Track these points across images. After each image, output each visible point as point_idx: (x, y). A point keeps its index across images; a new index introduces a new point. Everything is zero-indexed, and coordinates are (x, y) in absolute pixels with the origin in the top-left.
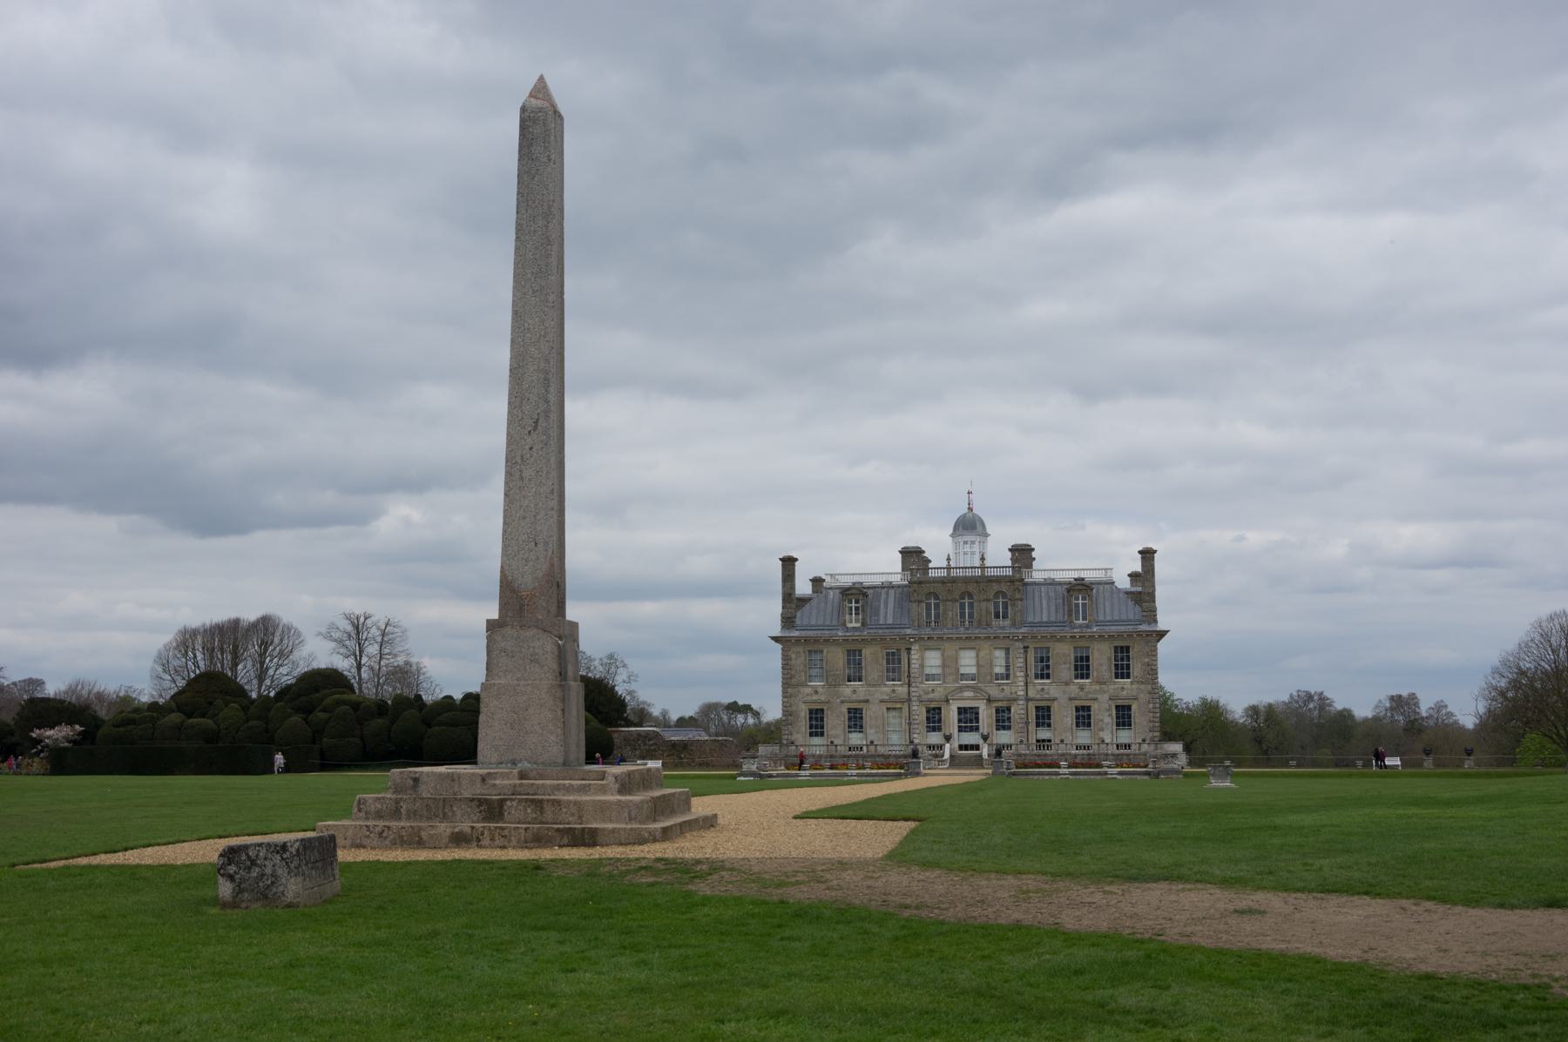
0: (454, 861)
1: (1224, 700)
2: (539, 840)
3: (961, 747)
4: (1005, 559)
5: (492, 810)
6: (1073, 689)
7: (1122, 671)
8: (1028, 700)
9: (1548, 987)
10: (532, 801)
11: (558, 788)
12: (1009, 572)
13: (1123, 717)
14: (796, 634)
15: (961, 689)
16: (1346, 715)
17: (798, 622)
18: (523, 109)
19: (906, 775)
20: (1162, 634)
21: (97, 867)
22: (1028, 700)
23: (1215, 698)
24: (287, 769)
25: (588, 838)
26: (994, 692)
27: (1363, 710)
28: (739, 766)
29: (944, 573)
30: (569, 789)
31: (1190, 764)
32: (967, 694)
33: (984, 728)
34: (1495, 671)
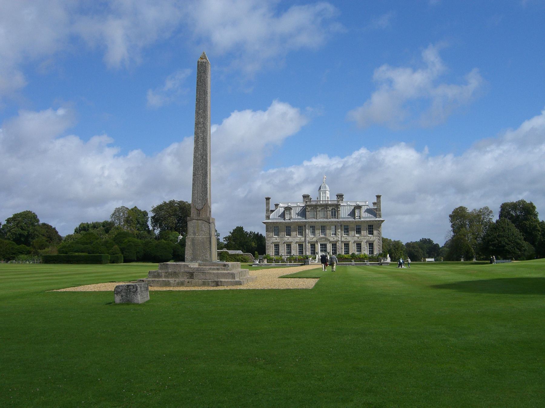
0: (230, 290)
1: (401, 241)
2: (204, 284)
4: (335, 198)
5: (191, 275)
6: (356, 239)
7: (371, 233)
8: (342, 242)
9: (504, 246)
11: (210, 269)
12: (336, 202)
14: (271, 221)
16: (437, 245)
17: (271, 217)
19: (304, 265)
20: (383, 221)
21: (78, 292)
22: (342, 242)
25: (217, 284)
26: (332, 239)
30: (214, 269)
31: (391, 261)
32: (323, 240)
34: (475, 210)
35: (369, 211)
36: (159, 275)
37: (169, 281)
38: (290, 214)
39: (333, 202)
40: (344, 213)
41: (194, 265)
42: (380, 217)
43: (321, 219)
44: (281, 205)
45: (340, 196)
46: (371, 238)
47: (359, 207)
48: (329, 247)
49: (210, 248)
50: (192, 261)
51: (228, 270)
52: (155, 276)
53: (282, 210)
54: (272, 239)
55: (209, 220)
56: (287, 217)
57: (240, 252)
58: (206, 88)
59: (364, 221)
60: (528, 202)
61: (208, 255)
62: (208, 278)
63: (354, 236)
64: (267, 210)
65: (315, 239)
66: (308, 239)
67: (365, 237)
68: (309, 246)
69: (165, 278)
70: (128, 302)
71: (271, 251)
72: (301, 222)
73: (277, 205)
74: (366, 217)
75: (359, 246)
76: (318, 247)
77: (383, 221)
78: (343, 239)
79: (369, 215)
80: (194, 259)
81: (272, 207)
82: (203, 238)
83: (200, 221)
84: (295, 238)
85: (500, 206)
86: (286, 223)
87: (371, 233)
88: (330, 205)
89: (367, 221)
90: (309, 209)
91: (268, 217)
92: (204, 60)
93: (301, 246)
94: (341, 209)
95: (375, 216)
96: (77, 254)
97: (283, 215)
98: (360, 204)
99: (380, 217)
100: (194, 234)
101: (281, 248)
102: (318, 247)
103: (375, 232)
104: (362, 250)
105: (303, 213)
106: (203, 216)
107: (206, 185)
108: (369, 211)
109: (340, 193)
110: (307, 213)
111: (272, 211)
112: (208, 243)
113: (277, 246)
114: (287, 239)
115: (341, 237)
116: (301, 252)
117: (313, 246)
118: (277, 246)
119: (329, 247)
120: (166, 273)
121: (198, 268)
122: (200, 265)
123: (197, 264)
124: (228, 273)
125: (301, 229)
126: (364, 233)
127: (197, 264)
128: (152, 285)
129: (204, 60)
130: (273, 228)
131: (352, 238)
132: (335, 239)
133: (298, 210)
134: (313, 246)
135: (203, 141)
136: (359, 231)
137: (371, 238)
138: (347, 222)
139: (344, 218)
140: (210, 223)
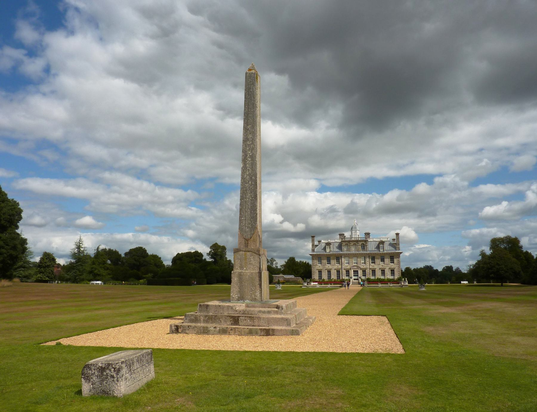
3: (354, 279)
4: (363, 236)
6: (381, 266)
8: (370, 269)
10: (250, 317)
11: (260, 311)
12: (364, 239)
13: (393, 272)
15: (354, 266)
16: (437, 270)
18: (246, 73)
20: (401, 253)
22: (370, 269)
23: (6, 192)
24: (197, 284)
26: (362, 267)
27: (440, 269)
28: (303, 284)
29: (349, 239)
30: (264, 312)
33: (360, 275)
35: (391, 245)
36: (196, 320)
37: (207, 327)
38: (330, 248)
39: (362, 239)
40: (371, 248)
41: (240, 306)
42: (399, 250)
43: (353, 250)
44: (323, 241)
45: (367, 234)
46: (392, 265)
47: (382, 242)
48: (360, 273)
49: (260, 285)
50: (238, 300)
51: (281, 313)
52: (192, 321)
53: (323, 245)
54: (317, 266)
55: (259, 251)
56: (328, 250)
57: (292, 277)
58: (255, 101)
59: (387, 253)
60: (513, 237)
61: (258, 294)
62: (256, 323)
63: (379, 265)
64: (313, 245)
65: (349, 267)
66: (343, 267)
67: (388, 265)
68: (344, 272)
69: (204, 323)
70: (105, 394)
71: (316, 276)
72: (338, 254)
73: (319, 242)
74: (387, 249)
75: (383, 272)
76: (352, 273)
77: (401, 253)
78: (371, 267)
79: (392, 248)
80: (241, 298)
81: (316, 243)
82: (252, 273)
83: (248, 253)
84: (334, 266)
85: (490, 241)
86: (327, 255)
87: (392, 262)
88: (361, 241)
89: (389, 253)
90: (344, 243)
91: (313, 250)
92: (253, 71)
93: (338, 272)
94: (369, 244)
95: (396, 249)
96: (172, 279)
97: (325, 249)
98: (384, 240)
99: (399, 250)
100: (241, 267)
101: (323, 273)
102: (352, 273)
103: (396, 260)
104: (386, 275)
105: (340, 247)
106: (252, 246)
107: (256, 210)
108: (391, 245)
109: (367, 231)
110: (343, 247)
111: (317, 246)
112: (257, 279)
113: (320, 272)
114: (328, 266)
115: (368, 265)
116: (338, 276)
117: (348, 272)
118: (320, 272)
119: (360, 273)
120: (206, 316)
121: (244, 312)
122: (247, 306)
123: (244, 305)
124: (282, 318)
125: (338, 258)
126: (387, 260)
127: (244, 305)
128: (187, 331)
129: (253, 71)
130: (318, 257)
131: (378, 265)
132: (365, 267)
133: (337, 245)
134: (348, 272)
135: (252, 160)
136: (383, 260)
137: (392, 265)
138: (373, 254)
139: (371, 251)
140: (260, 255)
